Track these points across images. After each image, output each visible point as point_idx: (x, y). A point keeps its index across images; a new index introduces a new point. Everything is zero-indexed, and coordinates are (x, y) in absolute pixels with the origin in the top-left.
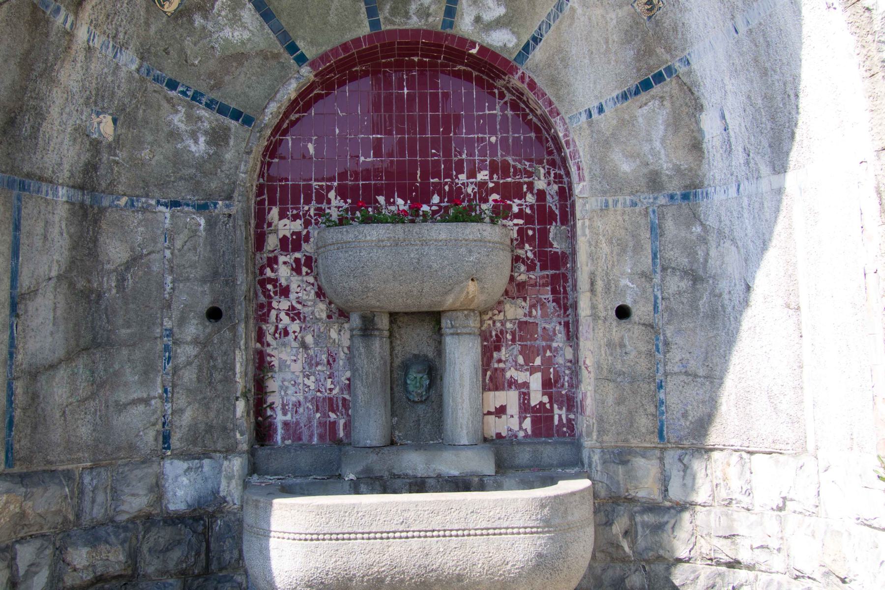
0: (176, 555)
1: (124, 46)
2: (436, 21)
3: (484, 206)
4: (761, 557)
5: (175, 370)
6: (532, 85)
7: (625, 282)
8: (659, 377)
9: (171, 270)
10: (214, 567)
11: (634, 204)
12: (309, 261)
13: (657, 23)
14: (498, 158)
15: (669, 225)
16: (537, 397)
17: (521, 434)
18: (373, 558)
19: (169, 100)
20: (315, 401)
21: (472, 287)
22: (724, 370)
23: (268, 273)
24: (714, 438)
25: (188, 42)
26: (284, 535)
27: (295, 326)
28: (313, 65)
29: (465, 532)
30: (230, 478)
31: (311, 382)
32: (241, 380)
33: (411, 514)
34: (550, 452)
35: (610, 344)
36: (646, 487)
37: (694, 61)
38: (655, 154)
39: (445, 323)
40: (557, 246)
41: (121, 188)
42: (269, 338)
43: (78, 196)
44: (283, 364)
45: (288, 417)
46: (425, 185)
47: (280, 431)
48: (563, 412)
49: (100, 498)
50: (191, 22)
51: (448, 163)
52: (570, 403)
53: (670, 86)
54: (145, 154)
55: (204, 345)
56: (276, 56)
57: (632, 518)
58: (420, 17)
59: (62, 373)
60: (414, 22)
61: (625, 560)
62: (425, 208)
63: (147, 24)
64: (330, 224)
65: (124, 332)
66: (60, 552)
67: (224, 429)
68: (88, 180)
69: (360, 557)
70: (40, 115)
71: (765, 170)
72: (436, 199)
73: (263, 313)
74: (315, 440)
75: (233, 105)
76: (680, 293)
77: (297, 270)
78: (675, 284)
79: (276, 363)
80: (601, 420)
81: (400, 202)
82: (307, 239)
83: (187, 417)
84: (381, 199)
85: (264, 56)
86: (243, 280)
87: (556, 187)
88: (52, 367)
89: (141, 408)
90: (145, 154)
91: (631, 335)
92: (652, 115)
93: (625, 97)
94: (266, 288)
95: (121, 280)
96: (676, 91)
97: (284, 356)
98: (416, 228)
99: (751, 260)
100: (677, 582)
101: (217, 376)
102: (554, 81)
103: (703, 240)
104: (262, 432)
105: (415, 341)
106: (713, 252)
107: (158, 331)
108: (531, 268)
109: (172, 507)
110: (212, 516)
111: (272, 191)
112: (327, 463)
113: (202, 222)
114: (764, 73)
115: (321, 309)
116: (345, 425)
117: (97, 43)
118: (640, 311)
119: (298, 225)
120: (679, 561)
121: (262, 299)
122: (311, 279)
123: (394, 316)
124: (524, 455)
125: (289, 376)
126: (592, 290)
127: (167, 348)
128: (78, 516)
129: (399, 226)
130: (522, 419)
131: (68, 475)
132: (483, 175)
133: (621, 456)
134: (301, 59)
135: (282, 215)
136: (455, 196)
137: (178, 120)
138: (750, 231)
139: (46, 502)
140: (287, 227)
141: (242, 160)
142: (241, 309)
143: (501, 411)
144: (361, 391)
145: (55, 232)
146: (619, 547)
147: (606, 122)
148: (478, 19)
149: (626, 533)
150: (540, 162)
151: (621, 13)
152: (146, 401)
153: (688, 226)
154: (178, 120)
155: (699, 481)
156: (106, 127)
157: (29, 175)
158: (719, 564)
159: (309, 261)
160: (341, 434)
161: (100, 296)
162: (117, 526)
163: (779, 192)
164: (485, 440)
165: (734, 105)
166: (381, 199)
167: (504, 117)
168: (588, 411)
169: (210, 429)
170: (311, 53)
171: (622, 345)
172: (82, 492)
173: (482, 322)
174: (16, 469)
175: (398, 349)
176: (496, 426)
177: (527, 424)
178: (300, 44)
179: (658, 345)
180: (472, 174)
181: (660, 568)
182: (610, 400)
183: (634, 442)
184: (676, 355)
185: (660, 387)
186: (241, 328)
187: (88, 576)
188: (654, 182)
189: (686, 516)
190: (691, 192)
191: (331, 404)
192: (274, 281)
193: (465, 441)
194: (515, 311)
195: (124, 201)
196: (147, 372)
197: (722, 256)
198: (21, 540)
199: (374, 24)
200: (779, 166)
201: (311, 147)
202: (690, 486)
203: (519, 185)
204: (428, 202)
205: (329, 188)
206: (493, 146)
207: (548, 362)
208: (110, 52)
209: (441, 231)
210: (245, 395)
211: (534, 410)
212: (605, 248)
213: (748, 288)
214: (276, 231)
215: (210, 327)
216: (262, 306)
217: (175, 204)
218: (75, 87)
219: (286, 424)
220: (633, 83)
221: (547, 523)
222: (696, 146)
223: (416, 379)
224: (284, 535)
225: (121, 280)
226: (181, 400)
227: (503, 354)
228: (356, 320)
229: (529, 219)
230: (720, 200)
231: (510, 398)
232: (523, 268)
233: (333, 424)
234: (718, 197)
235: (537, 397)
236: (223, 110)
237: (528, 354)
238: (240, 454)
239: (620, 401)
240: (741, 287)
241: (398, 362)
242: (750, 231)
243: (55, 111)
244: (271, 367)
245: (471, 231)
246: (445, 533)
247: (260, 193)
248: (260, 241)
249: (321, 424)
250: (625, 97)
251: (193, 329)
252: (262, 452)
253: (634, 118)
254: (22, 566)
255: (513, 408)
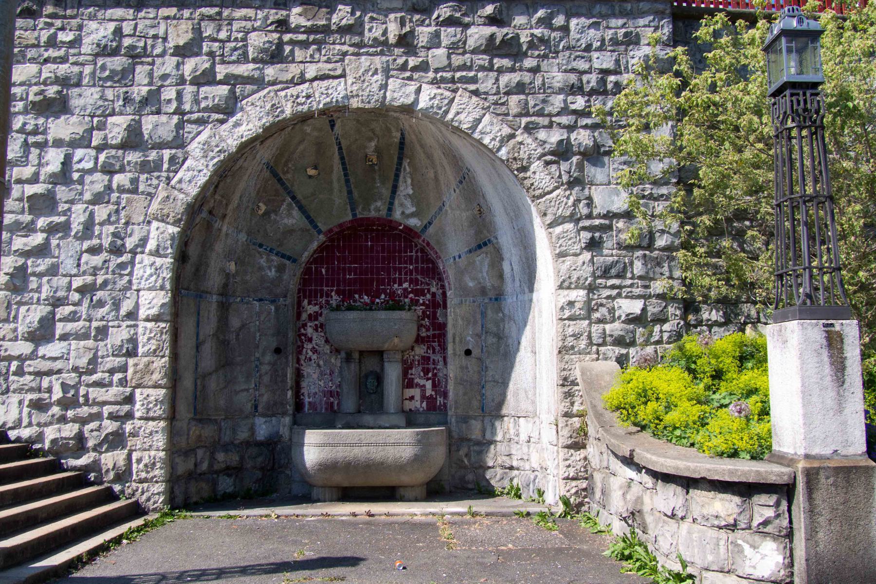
0: (260, 459)
1: (241, 231)
2: (383, 213)
3: (406, 300)
4: (521, 464)
5: (261, 376)
6: (428, 244)
7: (469, 338)
8: (483, 382)
9: (259, 331)
10: (276, 466)
11: (474, 302)
12: (322, 326)
13: (484, 220)
14: (413, 277)
15: (489, 312)
16: (429, 392)
17: (421, 409)
18: (346, 454)
19: (259, 252)
20: (324, 391)
21: (396, 340)
22: (509, 380)
23: (302, 331)
24: (504, 411)
25: (268, 226)
26: (310, 444)
27: (314, 357)
28: (325, 234)
29: (385, 444)
30: (284, 426)
31: (322, 383)
32: (290, 382)
33: (363, 437)
34: (433, 417)
35: (461, 368)
36: (476, 435)
37: (499, 237)
38: (484, 279)
39: (385, 356)
40: (441, 320)
41: (238, 294)
42: (302, 362)
43: (220, 298)
44: (309, 375)
45: (311, 400)
46: (378, 290)
47: (307, 406)
48: (442, 399)
49: (228, 433)
50: (270, 217)
51: (389, 279)
52: (445, 395)
53: (489, 248)
54: (248, 277)
55: (274, 365)
56: (308, 230)
57: (469, 448)
58: (376, 212)
59: (214, 377)
60: (373, 214)
61: (465, 467)
62: (377, 300)
63: (251, 220)
64: (333, 310)
65: (238, 359)
66: (212, 454)
67: (282, 404)
68: (225, 291)
69: (341, 453)
70: (208, 266)
71: (527, 290)
72: (383, 296)
73: (300, 350)
74: (323, 411)
75: (288, 254)
76: (493, 344)
77: (316, 330)
78: (491, 340)
79: (305, 374)
80: (456, 402)
81: (366, 297)
82: (321, 315)
83: (265, 398)
84: (357, 296)
85: (302, 230)
86: (291, 335)
87: (441, 291)
88: (210, 374)
89: (245, 393)
90: (248, 277)
91: (471, 363)
92: (482, 260)
93: (470, 251)
94: (302, 339)
95: (238, 335)
96: (492, 250)
97: (309, 370)
98: (371, 313)
99: (520, 331)
100: (488, 477)
101: (279, 379)
102: (438, 242)
103: (503, 320)
104: (299, 406)
105: (371, 364)
106: (506, 326)
107: (253, 358)
108: (428, 330)
109: (258, 438)
110: (276, 443)
111: (305, 291)
112: (330, 417)
113: (273, 308)
114: (525, 248)
115: (327, 349)
116: (338, 404)
117: (230, 232)
118: (475, 352)
119: (317, 308)
120: (489, 468)
121: (299, 343)
122: (322, 334)
123: (361, 353)
124: (421, 419)
125: (311, 380)
126: (454, 342)
127: (257, 366)
128: (219, 440)
129: (363, 312)
130: (422, 402)
131: (216, 420)
132: (406, 285)
133: (465, 420)
134: (320, 232)
135: (309, 303)
136: (392, 295)
137: (263, 261)
138: (521, 318)
139: (208, 431)
140: (312, 309)
141: (292, 279)
142: (290, 348)
143: (412, 398)
144: (345, 387)
145: (212, 315)
146: (463, 461)
147: (462, 262)
148: (403, 213)
149: (466, 455)
150: (433, 278)
151: (468, 213)
152: (247, 390)
153: (497, 313)
154: (263, 261)
155: (498, 431)
156: (232, 267)
157: (203, 292)
158: (506, 468)
159: (322, 326)
160: (336, 408)
161: (228, 344)
162: (235, 445)
163: (531, 300)
164: (403, 411)
165: (515, 259)
166: (357, 296)
167: (417, 256)
168: (450, 398)
169: (275, 404)
170: (324, 228)
171: (467, 368)
172: (221, 429)
173: (403, 356)
174: (197, 417)
175: (363, 368)
176: (408, 405)
177: (424, 404)
178: (319, 224)
179: (483, 368)
180: (400, 284)
181: (481, 471)
182: (461, 393)
183: (471, 413)
184: (490, 373)
185: (483, 387)
186: (290, 357)
187: (223, 466)
188: (483, 291)
189: (492, 447)
190: (498, 297)
191: (331, 394)
192: (305, 335)
193: (392, 411)
194: (420, 350)
195: (239, 299)
196: (248, 377)
197: (510, 328)
198: (198, 447)
199: (354, 215)
200: (531, 290)
201: (323, 271)
202: (494, 433)
203: (423, 290)
204: (379, 298)
205: (332, 291)
206: (411, 272)
207: (435, 375)
208: (235, 235)
209: (382, 315)
210: (291, 388)
211: (428, 398)
212: (460, 322)
213: (519, 343)
214: (306, 311)
215: (276, 357)
216: (299, 347)
217: (260, 300)
218: (220, 251)
219: (310, 403)
220: (474, 245)
221: (419, 442)
222: (501, 276)
223: (371, 382)
224: (310, 444)
225: (238, 335)
226: (263, 390)
227: (413, 371)
228: (343, 354)
229: (427, 306)
230: (510, 301)
231: (416, 392)
232: (424, 330)
233: (332, 403)
234: (509, 301)
235: (429, 392)
236: (283, 256)
237: (426, 371)
238: (289, 415)
239: (465, 394)
240: (516, 342)
241: (363, 374)
242: (521, 318)
243: (212, 263)
244: (303, 376)
245: (397, 314)
246: (377, 445)
247: (299, 293)
248: (299, 315)
249: (326, 403)
250: (470, 251)
251: (269, 357)
252: (298, 415)
253: (475, 261)
254: (199, 457)
255: (418, 397)
